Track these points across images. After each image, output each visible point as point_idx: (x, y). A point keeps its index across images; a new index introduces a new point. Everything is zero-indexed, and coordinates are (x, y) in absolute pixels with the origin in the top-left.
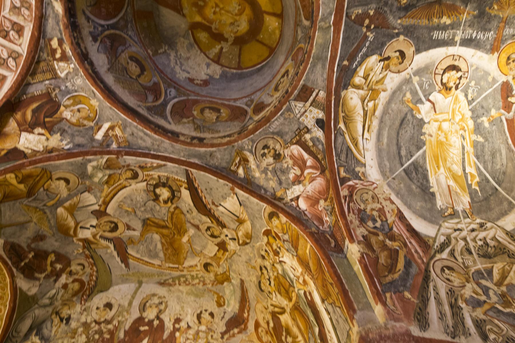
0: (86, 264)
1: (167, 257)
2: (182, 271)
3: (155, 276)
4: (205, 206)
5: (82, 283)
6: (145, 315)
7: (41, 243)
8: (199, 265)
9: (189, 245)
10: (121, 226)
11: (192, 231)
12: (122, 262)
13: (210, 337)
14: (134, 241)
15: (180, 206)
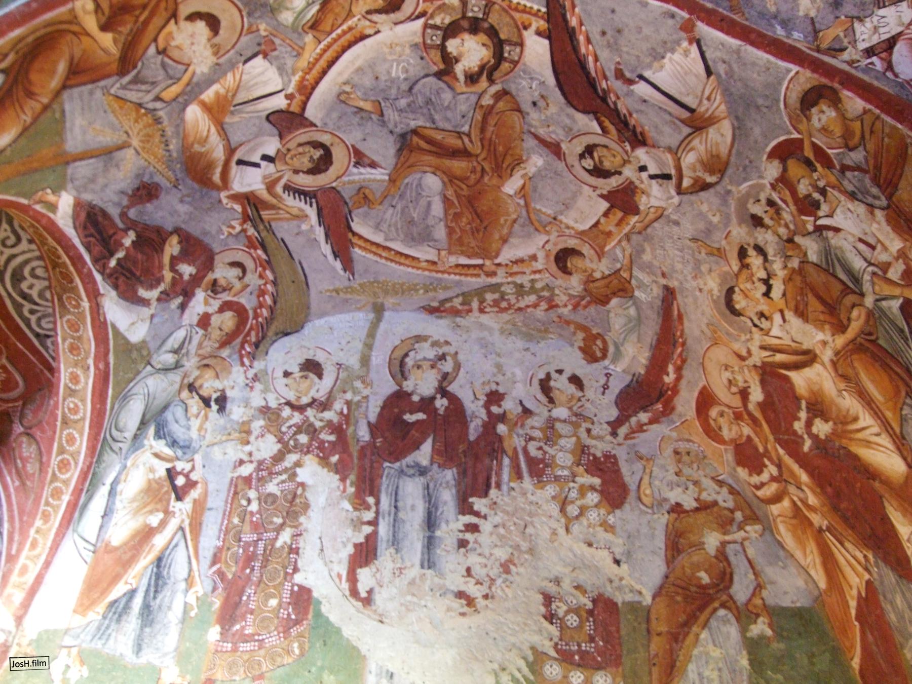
0: (249, 264)
1: (455, 237)
2: (494, 274)
3: (417, 291)
4: (592, 83)
5: (240, 311)
6: (408, 386)
7: (149, 207)
9: (522, 202)
10: (339, 155)
11: (537, 161)
12: (336, 256)
14: (370, 197)
15: (513, 88)
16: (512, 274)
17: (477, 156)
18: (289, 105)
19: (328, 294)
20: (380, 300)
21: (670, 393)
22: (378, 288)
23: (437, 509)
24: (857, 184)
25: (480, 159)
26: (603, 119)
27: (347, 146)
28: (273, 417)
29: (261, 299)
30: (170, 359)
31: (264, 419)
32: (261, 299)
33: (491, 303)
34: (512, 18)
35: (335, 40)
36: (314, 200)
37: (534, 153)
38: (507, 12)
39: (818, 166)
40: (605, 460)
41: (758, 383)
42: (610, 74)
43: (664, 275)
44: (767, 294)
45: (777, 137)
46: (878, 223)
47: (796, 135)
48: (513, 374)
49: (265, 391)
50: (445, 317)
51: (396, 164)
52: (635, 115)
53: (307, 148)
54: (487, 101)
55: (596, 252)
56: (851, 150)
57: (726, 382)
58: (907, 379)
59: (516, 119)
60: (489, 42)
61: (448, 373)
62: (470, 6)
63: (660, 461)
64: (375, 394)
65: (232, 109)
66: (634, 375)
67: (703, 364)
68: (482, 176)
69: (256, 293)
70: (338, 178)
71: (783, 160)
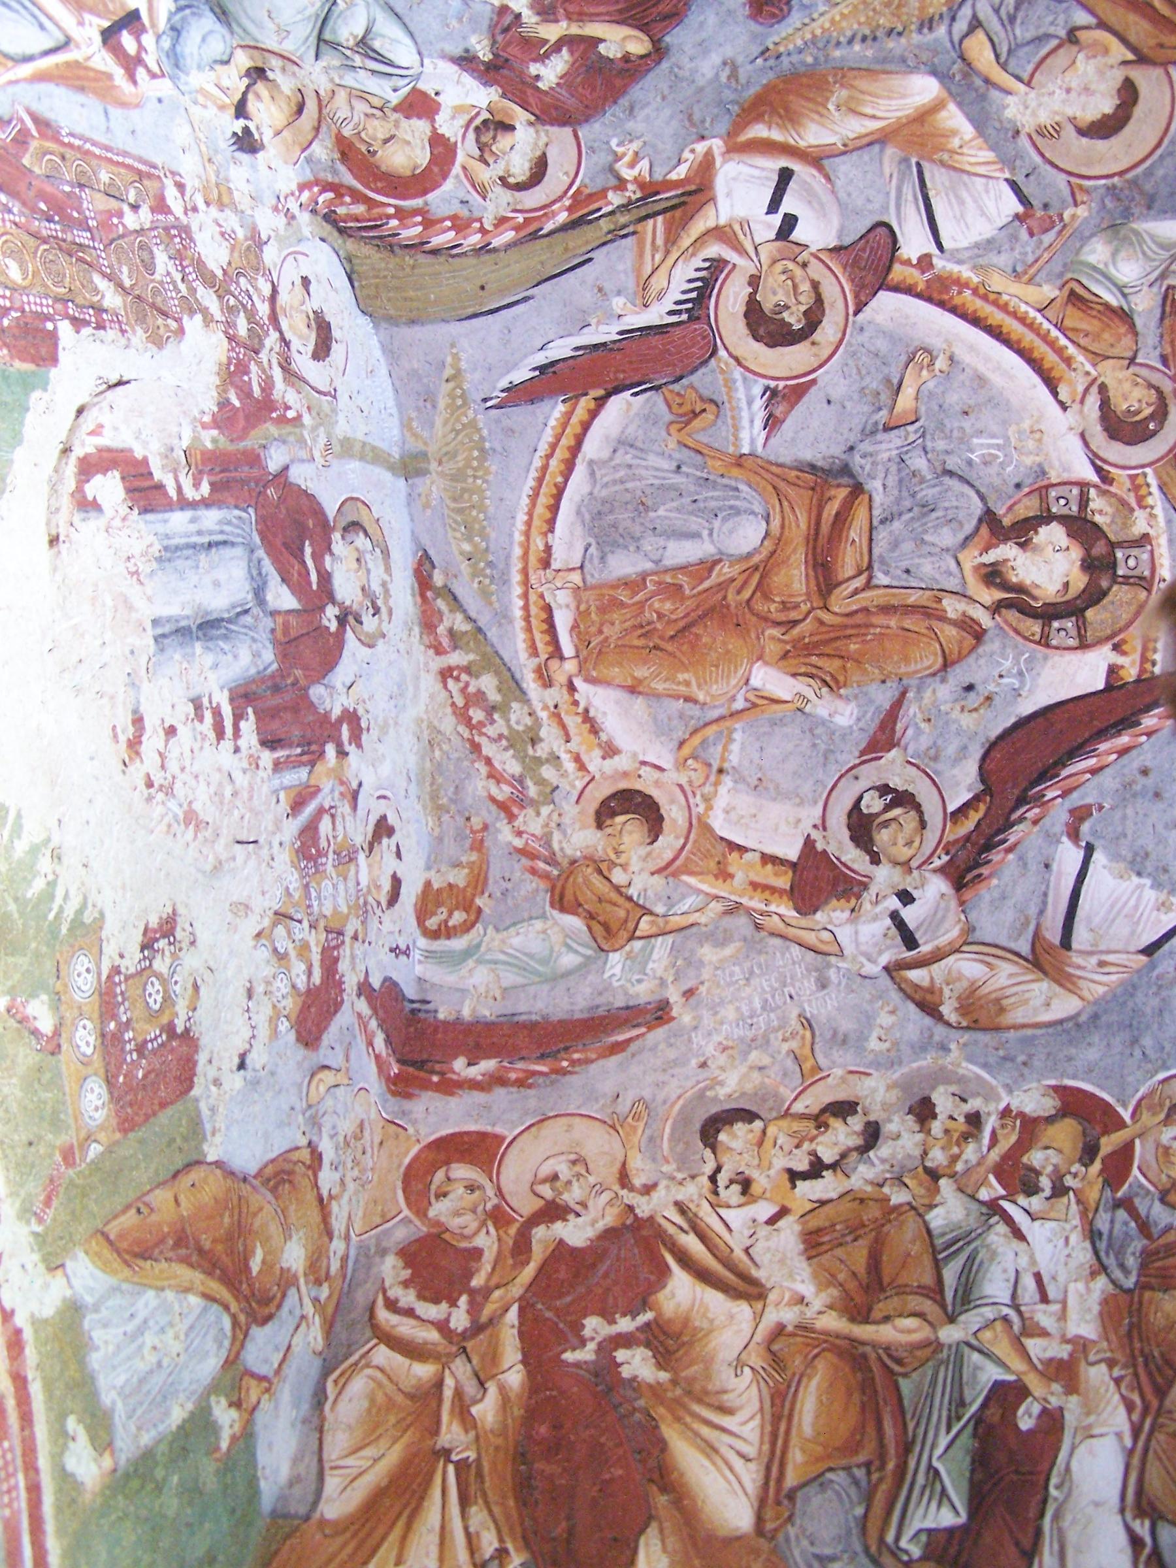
0: (533, 198)
1: (623, 596)
2: (546, 682)
4: (1046, 774)
9: (739, 704)
12: (542, 369)
14: (696, 423)
15: (991, 645)
16: (557, 716)
18: (908, 262)
19: (449, 359)
20: (433, 466)
22: (468, 460)
23: (225, 637)
24: (1116, 1231)
25: (820, 613)
26: (982, 808)
27: (814, 371)
29: (448, 223)
33: (471, 689)
35: (1045, 338)
36: (684, 317)
39: (1097, 1166)
41: (601, 1225)
42: (1075, 799)
44: (794, 1176)
46: (1088, 1289)
47: (1126, 1115)
52: (1011, 856)
53: (807, 300)
54: (952, 607)
56: (1162, 1200)
58: (337, 1560)
59: (927, 663)
60: (1073, 592)
62: (1134, 552)
68: (778, 624)
69: (464, 213)
70: (737, 359)
71: (1064, 1112)
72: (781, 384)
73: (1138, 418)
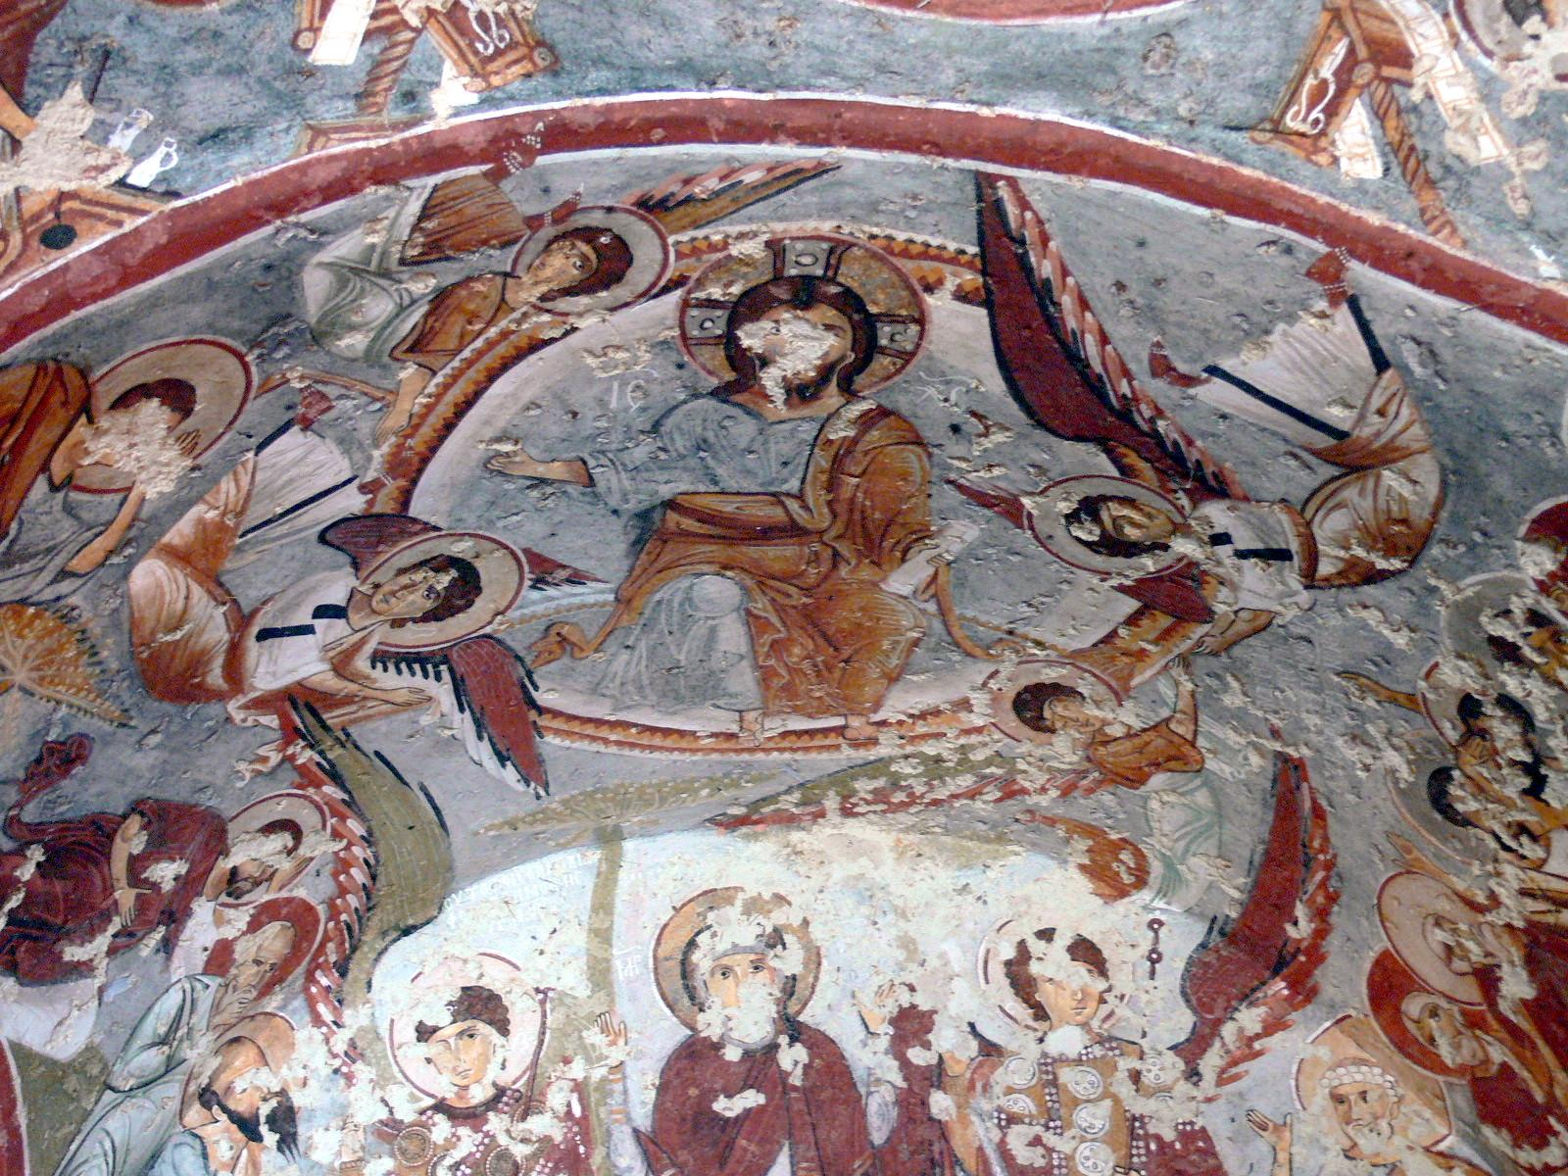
0: (307, 817)
2: (873, 741)
4: (1094, 386)
5: (300, 917)
6: (710, 1025)
7: (67, 785)
8: (979, 700)
9: (932, 607)
10: (494, 572)
12: (502, 759)
13: (1125, 1089)
16: (913, 739)
17: (821, 533)
18: (371, 503)
21: (1302, 958)
25: (826, 538)
27: (513, 554)
28: (412, 1147)
29: (342, 878)
30: (154, 1058)
31: (392, 1155)
32: (342, 878)
34: (896, 270)
36: (443, 668)
37: (957, 518)
38: (881, 259)
40: (1185, 1145)
42: (1139, 367)
43: (1275, 734)
45: (1557, 494)
48: (942, 956)
49: (381, 1082)
50: (764, 834)
51: (632, 569)
52: (1199, 443)
54: (840, 432)
55: (1110, 687)
57: (1440, 950)
59: (913, 457)
61: (794, 978)
63: (1304, 1129)
64: (640, 1055)
65: (238, 541)
66: (1214, 920)
67: (1379, 906)
68: (835, 566)
72: (528, 576)
73: (593, 257)
